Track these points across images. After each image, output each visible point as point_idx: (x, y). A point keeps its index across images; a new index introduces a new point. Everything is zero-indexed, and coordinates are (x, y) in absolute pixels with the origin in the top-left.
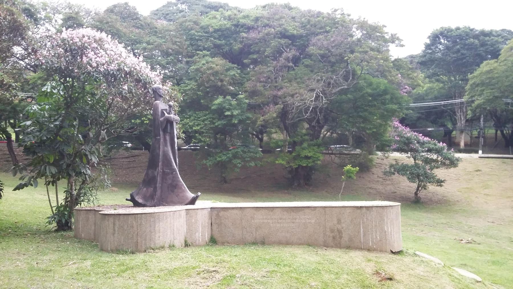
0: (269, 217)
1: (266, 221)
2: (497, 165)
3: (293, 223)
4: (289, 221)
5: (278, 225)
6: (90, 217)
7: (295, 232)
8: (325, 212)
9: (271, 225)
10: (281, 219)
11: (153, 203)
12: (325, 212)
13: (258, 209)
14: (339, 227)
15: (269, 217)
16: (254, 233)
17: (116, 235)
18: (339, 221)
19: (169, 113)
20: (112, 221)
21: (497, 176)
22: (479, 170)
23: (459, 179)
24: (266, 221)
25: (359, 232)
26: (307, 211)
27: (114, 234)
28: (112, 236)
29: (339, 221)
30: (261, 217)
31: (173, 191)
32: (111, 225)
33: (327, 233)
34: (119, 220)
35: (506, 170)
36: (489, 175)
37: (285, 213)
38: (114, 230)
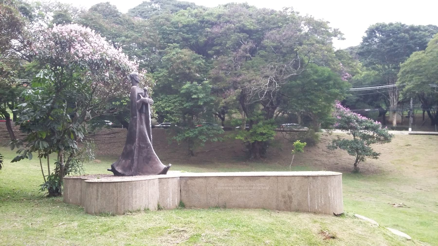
0: (230, 185)
1: (227, 188)
2: (425, 141)
3: (250, 189)
4: (247, 188)
5: (237, 192)
6: (77, 184)
7: (252, 198)
8: (277, 180)
9: (232, 191)
10: (240, 186)
11: (130, 173)
12: (277, 180)
13: (221, 178)
14: (290, 193)
15: (230, 185)
16: (217, 199)
17: (99, 200)
18: (289, 188)
19: (144, 97)
20: (96, 188)
21: (425, 149)
22: (409, 145)
23: (392, 153)
24: (227, 188)
25: (307, 197)
26: (262, 179)
27: (97, 199)
28: (96, 201)
29: (289, 188)
30: (223, 185)
31: (148, 163)
32: (95, 192)
33: (279, 199)
34: (102, 187)
35: (432, 145)
36: (417, 149)
37: (243, 181)
38: (98, 196)
